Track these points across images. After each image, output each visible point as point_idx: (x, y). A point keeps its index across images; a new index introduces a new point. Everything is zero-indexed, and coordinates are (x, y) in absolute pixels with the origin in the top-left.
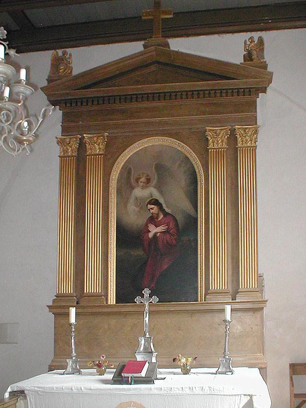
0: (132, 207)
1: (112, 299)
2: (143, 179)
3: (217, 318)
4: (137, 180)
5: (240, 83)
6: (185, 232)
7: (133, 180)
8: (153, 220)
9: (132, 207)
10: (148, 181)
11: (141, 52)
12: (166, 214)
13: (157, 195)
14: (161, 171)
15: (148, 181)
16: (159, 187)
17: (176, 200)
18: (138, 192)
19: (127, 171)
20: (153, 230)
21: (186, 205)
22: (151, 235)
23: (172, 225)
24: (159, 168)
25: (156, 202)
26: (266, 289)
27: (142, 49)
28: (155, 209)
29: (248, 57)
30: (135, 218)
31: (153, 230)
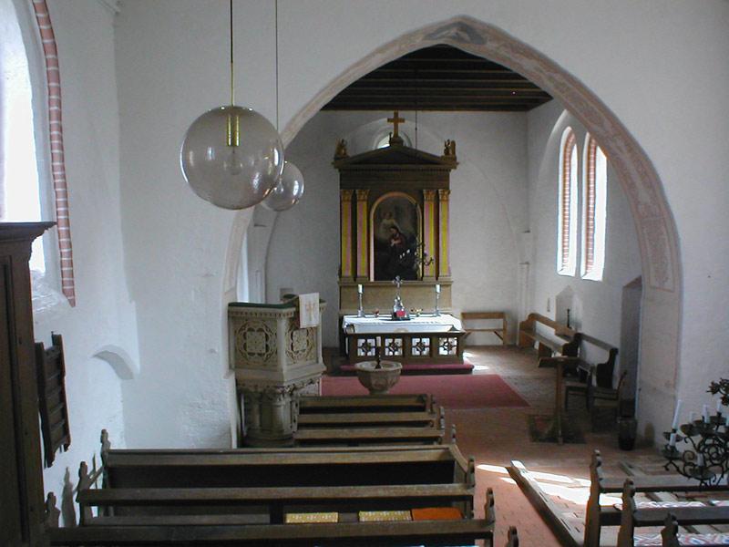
0: (382, 230)
1: (372, 279)
2: (388, 214)
3: (432, 289)
4: (385, 214)
5: (442, 167)
6: (411, 241)
7: (382, 215)
8: (393, 237)
9: (382, 230)
10: (391, 215)
11: (401, 110)
12: (400, 234)
13: (395, 224)
14: (397, 211)
15: (391, 215)
16: (397, 219)
17: (406, 226)
18: (385, 221)
19: (378, 209)
20: (394, 242)
21: (411, 229)
22: (392, 245)
23: (404, 240)
24: (397, 208)
25: (395, 227)
26: (452, 275)
27: (37, 340)
28: (394, 231)
29: (447, 151)
30: (383, 236)
31: (394, 242)
